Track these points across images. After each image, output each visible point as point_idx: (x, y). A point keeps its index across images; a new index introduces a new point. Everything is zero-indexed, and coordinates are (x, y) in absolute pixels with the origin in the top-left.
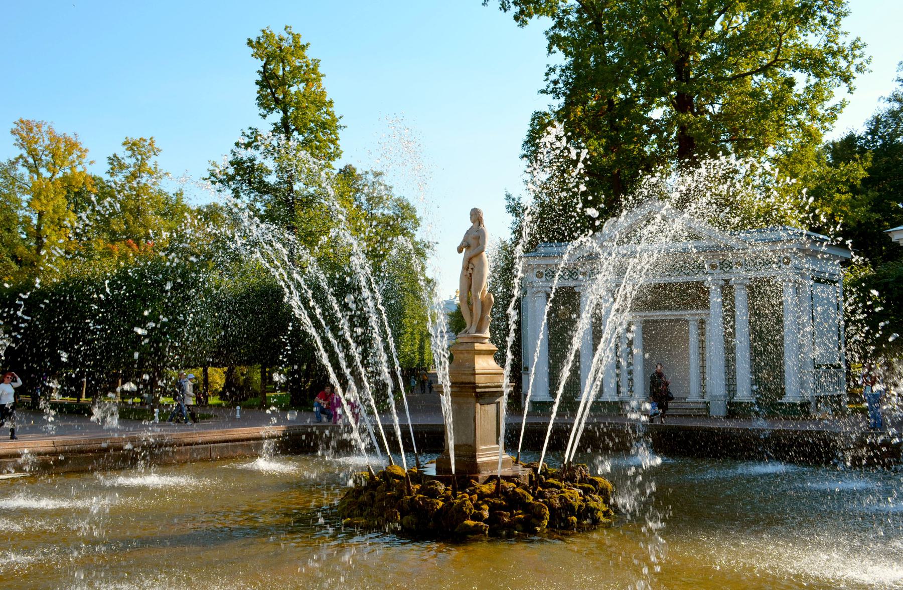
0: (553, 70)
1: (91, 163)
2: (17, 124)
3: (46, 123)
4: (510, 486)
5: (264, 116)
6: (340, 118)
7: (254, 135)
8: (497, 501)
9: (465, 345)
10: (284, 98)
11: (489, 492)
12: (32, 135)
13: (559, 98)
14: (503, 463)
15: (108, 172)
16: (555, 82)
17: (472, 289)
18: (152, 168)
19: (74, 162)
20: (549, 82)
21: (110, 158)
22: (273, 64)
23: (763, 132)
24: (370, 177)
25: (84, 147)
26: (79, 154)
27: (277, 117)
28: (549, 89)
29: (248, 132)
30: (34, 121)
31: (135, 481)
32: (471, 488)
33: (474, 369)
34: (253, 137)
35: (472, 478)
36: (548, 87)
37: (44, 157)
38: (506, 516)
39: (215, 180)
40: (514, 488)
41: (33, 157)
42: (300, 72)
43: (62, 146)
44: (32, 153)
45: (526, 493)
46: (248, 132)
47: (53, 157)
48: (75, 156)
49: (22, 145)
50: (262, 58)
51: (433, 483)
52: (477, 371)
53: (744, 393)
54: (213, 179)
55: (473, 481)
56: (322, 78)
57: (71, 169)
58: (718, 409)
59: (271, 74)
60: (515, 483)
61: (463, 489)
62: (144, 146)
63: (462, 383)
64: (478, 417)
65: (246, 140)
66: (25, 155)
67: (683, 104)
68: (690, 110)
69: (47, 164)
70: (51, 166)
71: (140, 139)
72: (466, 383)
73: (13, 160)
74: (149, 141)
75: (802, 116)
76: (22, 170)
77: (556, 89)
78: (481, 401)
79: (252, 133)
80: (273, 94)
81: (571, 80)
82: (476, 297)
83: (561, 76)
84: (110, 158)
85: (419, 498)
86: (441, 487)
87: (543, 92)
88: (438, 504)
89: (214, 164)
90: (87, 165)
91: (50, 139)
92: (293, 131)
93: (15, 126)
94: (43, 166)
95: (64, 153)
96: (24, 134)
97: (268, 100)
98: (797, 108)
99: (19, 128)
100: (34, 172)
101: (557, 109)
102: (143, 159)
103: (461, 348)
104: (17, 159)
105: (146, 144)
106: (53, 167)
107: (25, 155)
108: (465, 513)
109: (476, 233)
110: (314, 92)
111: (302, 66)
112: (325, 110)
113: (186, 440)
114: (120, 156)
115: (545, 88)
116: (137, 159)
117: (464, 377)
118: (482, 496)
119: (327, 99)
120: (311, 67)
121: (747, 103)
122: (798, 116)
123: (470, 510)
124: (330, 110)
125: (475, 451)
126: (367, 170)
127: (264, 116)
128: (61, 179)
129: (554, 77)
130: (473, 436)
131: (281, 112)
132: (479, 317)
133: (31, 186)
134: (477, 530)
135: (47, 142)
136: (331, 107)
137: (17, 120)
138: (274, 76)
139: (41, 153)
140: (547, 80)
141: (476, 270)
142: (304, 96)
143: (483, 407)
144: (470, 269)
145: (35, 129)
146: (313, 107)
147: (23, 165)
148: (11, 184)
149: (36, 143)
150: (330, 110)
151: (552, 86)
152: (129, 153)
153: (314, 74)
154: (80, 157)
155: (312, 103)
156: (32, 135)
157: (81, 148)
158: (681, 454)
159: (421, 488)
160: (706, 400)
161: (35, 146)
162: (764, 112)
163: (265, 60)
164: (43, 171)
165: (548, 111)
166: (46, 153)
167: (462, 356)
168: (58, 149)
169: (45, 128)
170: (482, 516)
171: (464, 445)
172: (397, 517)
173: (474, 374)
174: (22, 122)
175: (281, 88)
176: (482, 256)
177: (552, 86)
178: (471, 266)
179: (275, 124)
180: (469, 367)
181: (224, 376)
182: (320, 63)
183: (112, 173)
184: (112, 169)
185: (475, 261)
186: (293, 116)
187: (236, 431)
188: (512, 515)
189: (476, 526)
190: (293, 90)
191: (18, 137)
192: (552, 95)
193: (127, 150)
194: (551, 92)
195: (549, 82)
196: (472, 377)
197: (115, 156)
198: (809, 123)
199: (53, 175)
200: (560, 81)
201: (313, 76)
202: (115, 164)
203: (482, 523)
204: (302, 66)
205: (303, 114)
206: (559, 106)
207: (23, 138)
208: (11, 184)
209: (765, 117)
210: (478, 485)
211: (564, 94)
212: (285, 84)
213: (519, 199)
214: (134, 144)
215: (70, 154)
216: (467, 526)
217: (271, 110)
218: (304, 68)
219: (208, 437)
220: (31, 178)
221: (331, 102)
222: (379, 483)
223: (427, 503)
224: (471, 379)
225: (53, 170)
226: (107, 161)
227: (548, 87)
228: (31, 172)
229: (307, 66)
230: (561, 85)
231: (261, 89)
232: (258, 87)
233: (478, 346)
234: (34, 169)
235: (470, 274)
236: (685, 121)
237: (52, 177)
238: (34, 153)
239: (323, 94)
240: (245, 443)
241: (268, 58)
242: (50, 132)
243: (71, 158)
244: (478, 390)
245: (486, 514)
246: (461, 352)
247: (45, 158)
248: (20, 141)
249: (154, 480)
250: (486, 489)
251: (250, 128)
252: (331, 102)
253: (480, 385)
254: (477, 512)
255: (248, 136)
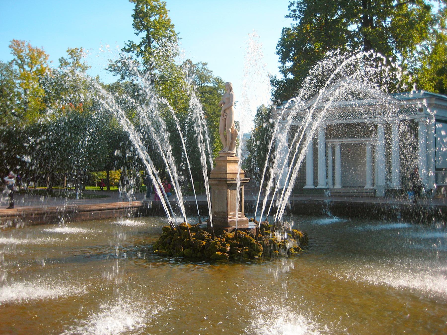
0: (292, 4)
1: (51, 62)
2: (12, 42)
3: (26, 41)
4: (243, 234)
5: (137, 34)
6: (178, 33)
7: (131, 44)
8: (235, 242)
9: (222, 158)
10: (147, 24)
11: (232, 237)
12: (19, 48)
13: (297, 20)
14: (238, 222)
15: (59, 67)
16: (294, 11)
17: (226, 128)
18: (82, 64)
19: (42, 62)
20: (290, 11)
21: (60, 60)
22: (141, 5)
23: (411, 37)
24: (200, 66)
25: (47, 54)
26: (44, 57)
27: (144, 34)
28: (291, 15)
29: (128, 43)
30: (20, 40)
31: (58, 230)
32: (223, 235)
33: (227, 171)
34: (131, 45)
35: (224, 230)
36: (290, 14)
37: (26, 60)
38: (239, 250)
39: (111, 69)
40: (245, 235)
41: (21, 60)
42: (155, 9)
43: (36, 54)
44: (20, 57)
45: (251, 238)
46: (128, 43)
47: (31, 59)
48: (42, 58)
49: (15, 53)
50: (135, 2)
51: (202, 232)
52: (228, 172)
53: (396, 184)
54: (110, 69)
55: (224, 231)
56: (168, 12)
57: (41, 65)
58: (381, 193)
59: (140, 11)
60: (246, 232)
61: (217, 235)
62: (77, 52)
63: (220, 178)
64: (229, 197)
65: (127, 47)
66: (17, 59)
67: (367, 22)
68: (370, 25)
69: (28, 63)
70: (30, 64)
71: (76, 48)
72: (222, 178)
73: (10, 61)
74: (80, 50)
75: (436, 27)
76: (16, 67)
77: (295, 15)
78: (230, 188)
79: (130, 44)
80: (141, 21)
81: (303, 10)
82: (228, 131)
83: (297, 7)
84: (60, 60)
85: (193, 240)
86: (206, 235)
87: (287, 16)
88: (203, 243)
89: (111, 61)
90: (49, 63)
91: (29, 50)
92: (153, 41)
93: (10, 44)
94: (26, 65)
95: (36, 57)
96: (16, 47)
97: (139, 25)
98: (433, 21)
99: (13, 44)
100: (21, 67)
101: (295, 26)
102: (77, 59)
103: (220, 159)
104: (12, 61)
105: (78, 51)
106: (31, 65)
107: (17, 59)
108: (216, 248)
109: (228, 96)
110: (164, 20)
111: (157, 6)
112: (170, 29)
113: (88, 209)
114: (65, 58)
115: (289, 14)
116: (74, 59)
117: (221, 175)
118: (227, 239)
119: (171, 24)
120: (162, 6)
121: (402, 20)
122: (434, 27)
123: (219, 246)
124: (173, 29)
125: (227, 215)
126: (199, 62)
127: (137, 34)
128: (35, 71)
129: (293, 8)
130: (226, 207)
131: (146, 31)
132: (230, 142)
133: (20, 75)
134: (222, 257)
135: (28, 52)
136: (173, 28)
137: (12, 40)
138: (141, 11)
139: (25, 57)
140: (290, 9)
141: (228, 116)
142: (158, 22)
143: (231, 191)
144: (225, 116)
145: (21, 45)
146: (164, 29)
147: (16, 64)
148: (10, 75)
149: (22, 52)
150: (173, 29)
151: (292, 13)
152: (70, 56)
153: (163, 10)
154: (45, 59)
155: (163, 26)
156: (19, 48)
157: (45, 54)
158: (348, 217)
159: (196, 234)
160: (375, 188)
161: (22, 54)
162: (411, 24)
163: (136, 3)
164: (26, 67)
165: (290, 27)
166: (27, 57)
167: (220, 163)
168: (34, 55)
169: (26, 44)
170: (226, 249)
171: (222, 212)
172: (182, 250)
173: (227, 173)
174: (14, 41)
175: (145, 19)
176: (231, 108)
177: (292, 13)
178: (225, 114)
179: (143, 38)
180: (224, 170)
181: (120, 175)
182: (166, 4)
183: (61, 67)
184: (61, 65)
185: (227, 112)
186: (152, 34)
187: (114, 204)
188: (243, 249)
189: (222, 255)
190: (152, 19)
191: (12, 49)
192: (293, 18)
193: (69, 54)
194: (292, 16)
195: (290, 11)
196: (225, 175)
197: (62, 58)
198: (441, 31)
199: (32, 69)
200: (297, 10)
201: (163, 11)
202: (63, 62)
203: (225, 254)
204: (157, 6)
205: (157, 32)
206: (297, 24)
207: (15, 50)
208: (10, 75)
209: (412, 28)
210: (226, 233)
211: (300, 17)
212: (148, 16)
213: (275, 77)
214: (72, 51)
215: (40, 58)
216: (217, 255)
217: (141, 30)
218: (158, 7)
219: (99, 208)
220: (20, 71)
221: (173, 25)
222: (176, 232)
223: (196, 243)
224: (225, 176)
225: (31, 67)
226: (58, 61)
227: (290, 14)
228: (19, 68)
229: (159, 6)
230: (298, 13)
231: (135, 19)
232: (133, 18)
233: (229, 158)
234: (21, 66)
235: (225, 119)
236: (366, 32)
237: (31, 70)
238: (21, 58)
239: (169, 21)
240: (111, 211)
241: (138, 3)
242: (29, 46)
243: (40, 60)
244: (228, 182)
245: (228, 249)
246: (220, 161)
247: (27, 60)
248: (14, 51)
249: (66, 229)
250: (230, 235)
251: (129, 41)
252: (173, 25)
253: (229, 179)
254: (223, 247)
255: (128, 45)
